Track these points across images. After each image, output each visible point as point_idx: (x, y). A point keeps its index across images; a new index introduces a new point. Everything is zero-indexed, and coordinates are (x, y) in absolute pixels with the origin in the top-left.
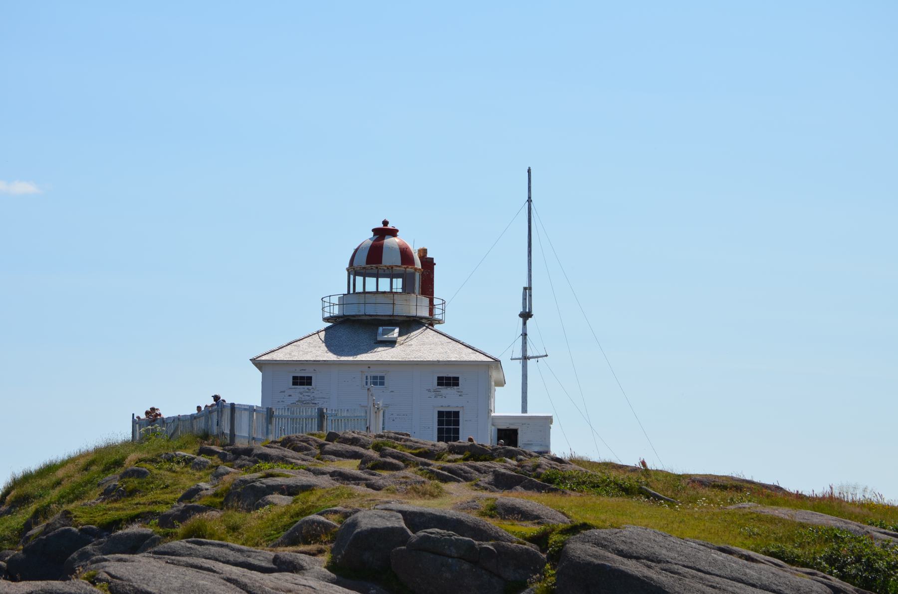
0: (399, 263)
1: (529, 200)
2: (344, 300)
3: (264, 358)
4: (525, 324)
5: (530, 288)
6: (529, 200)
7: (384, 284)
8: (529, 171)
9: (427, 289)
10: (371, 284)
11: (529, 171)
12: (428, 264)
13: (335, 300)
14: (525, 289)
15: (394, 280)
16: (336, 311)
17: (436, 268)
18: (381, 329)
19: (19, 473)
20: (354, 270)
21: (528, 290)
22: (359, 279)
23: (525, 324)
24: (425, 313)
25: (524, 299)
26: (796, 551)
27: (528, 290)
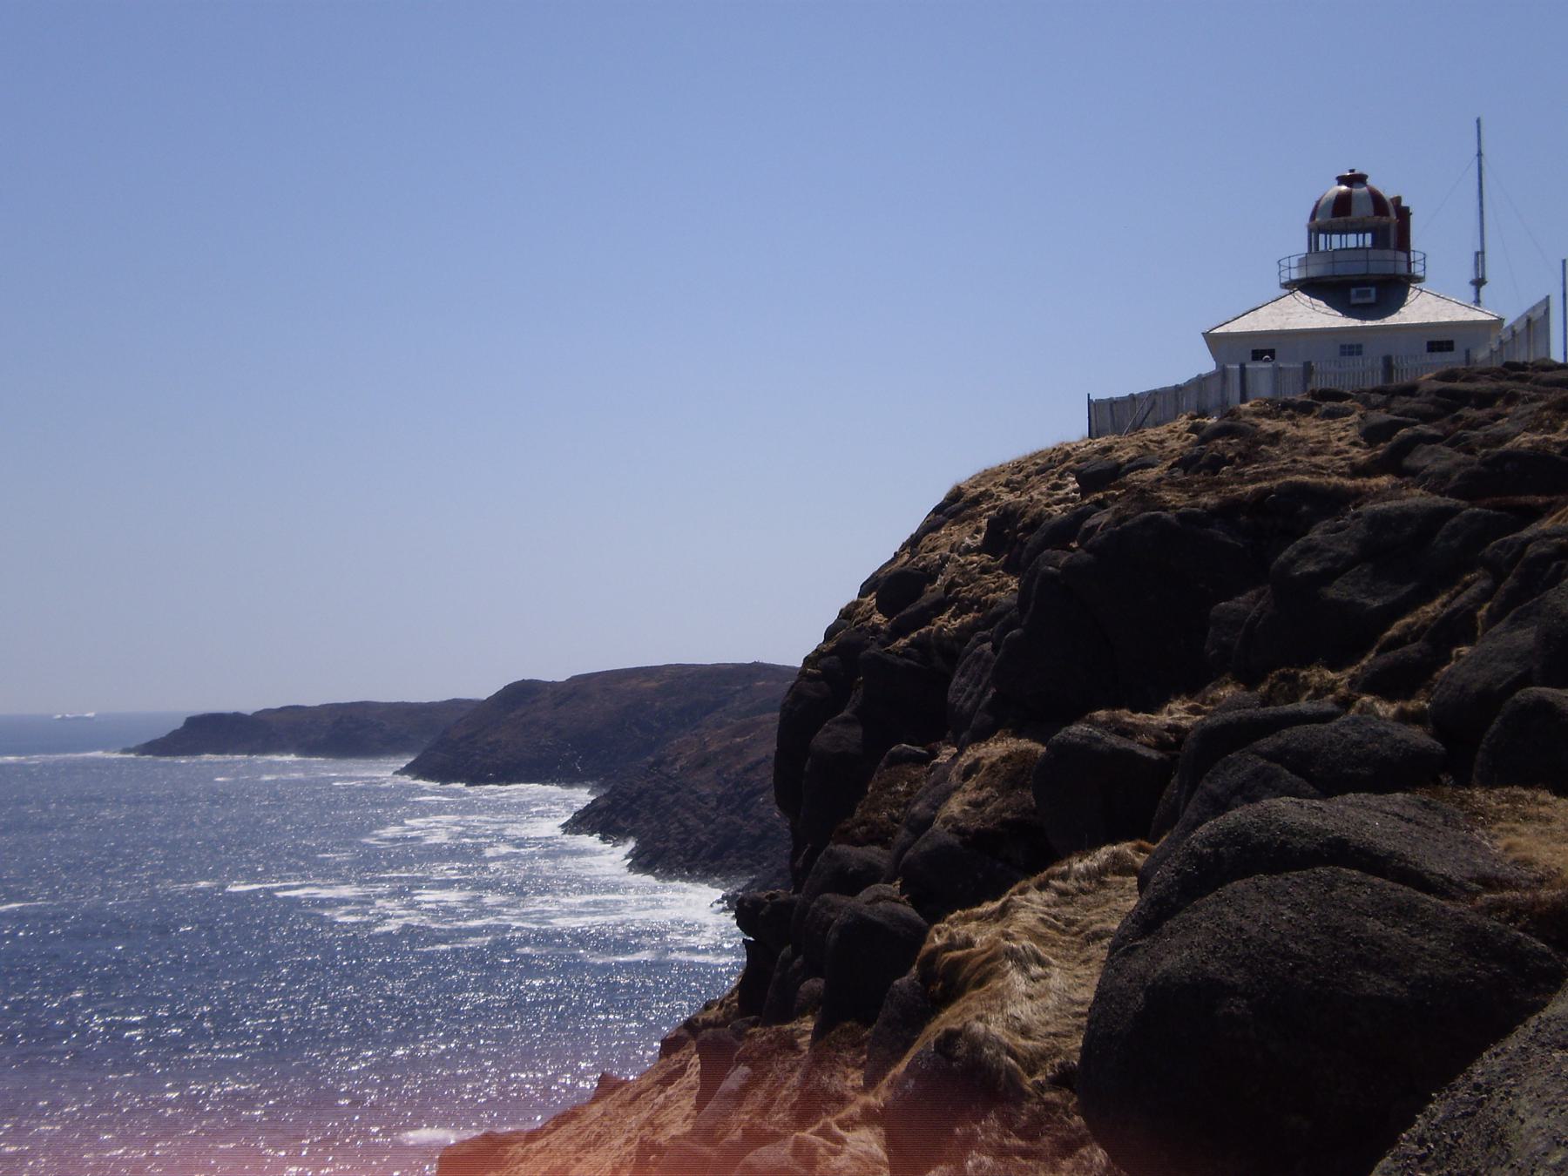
0: (1371, 213)
1: (1480, 154)
2: (1304, 263)
3: (1234, 327)
4: (1478, 292)
5: (1483, 252)
6: (1480, 154)
7: (1352, 240)
8: (1478, 121)
9: (1403, 243)
10: (1336, 241)
11: (1478, 121)
12: (1404, 214)
13: (1294, 262)
14: (1477, 254)
15: (1322, 237)
16: (1295, 275)
17: (1413, 219)
18: (1353, 291)
19: (844, 605)
20: (1315, 230)
21: (1480, 256)
22: (1322, 237)
23: (1478, 292)
24: (1403, 270)
25: (1476, 264)
26: (1204, 499)
27: (1480, 256)
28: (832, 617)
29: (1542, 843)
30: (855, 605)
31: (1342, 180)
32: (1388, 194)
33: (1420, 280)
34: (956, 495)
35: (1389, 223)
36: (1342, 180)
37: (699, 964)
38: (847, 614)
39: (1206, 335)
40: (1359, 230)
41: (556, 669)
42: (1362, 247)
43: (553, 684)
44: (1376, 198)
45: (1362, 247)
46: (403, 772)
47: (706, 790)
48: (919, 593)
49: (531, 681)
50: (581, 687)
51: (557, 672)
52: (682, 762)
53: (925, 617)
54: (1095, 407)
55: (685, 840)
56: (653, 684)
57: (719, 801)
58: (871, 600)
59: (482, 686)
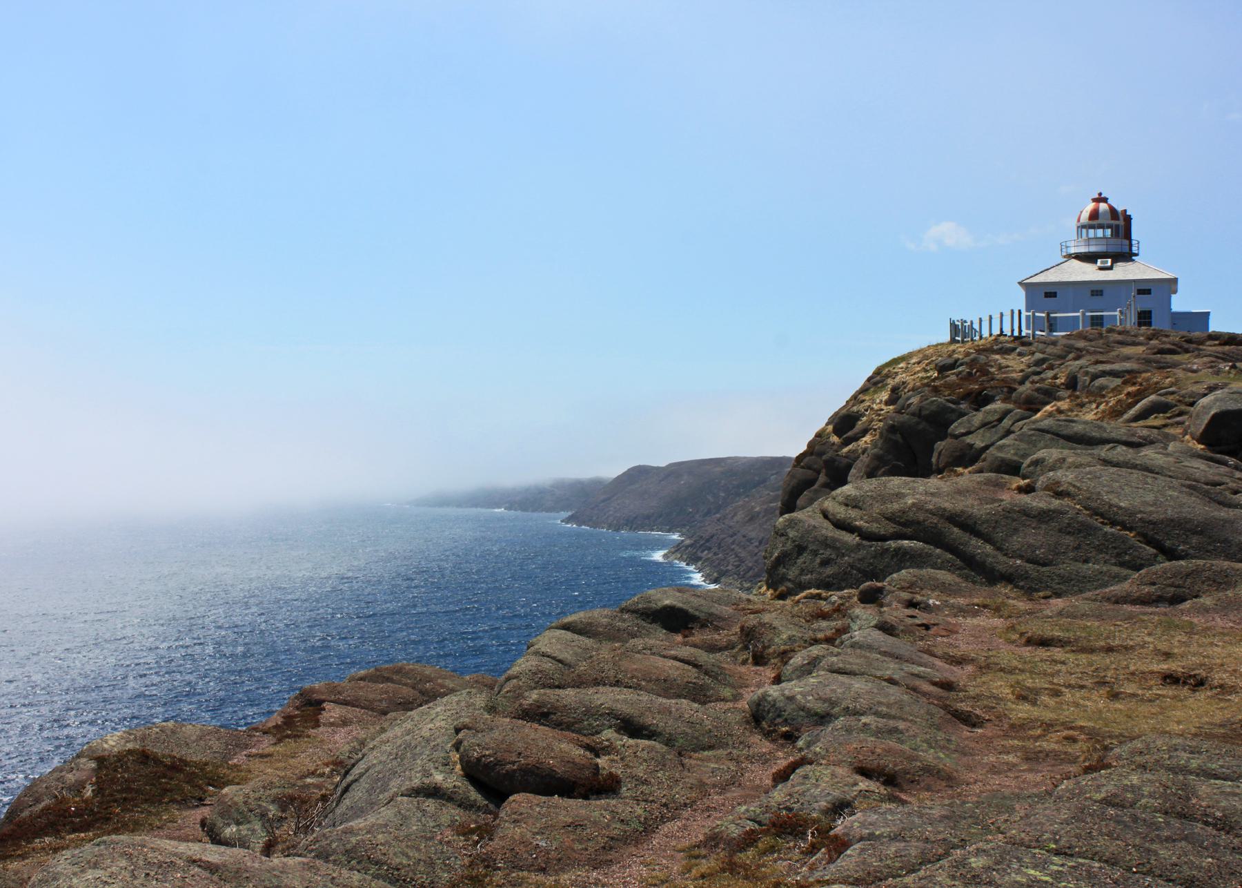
9: (1128, 235)
12: (1128, 219)
22: (1084, 231)
28: (811, 436)
29: (871, 564)
30: (823, 430)
31: (1094, 200)
32: (1120, 209)
33: (1136, 255)
34: (878, 372)
35: (1120, 224)
36: (1094, 200)
37: (1015, 738)
38: (819, 435)
39: (1020, 283)
40: (1101, 226)
41: (660, 459)
42: (1114, 232)
43: (658, 468)
44: (1113, 211)
45: (1114, 232)
46: (568, 520)
47: (753, 534)
48: (853, 426)
49: (644, 467)
50: (676, 470)
51: (661, 461)
52: (738, 518)
53: (856, 438)
54: (1030, 288)
55: (738, 566)
56: (718, 469)
57: (760, 542)
58: (830, 428)
59: (612, 470)
